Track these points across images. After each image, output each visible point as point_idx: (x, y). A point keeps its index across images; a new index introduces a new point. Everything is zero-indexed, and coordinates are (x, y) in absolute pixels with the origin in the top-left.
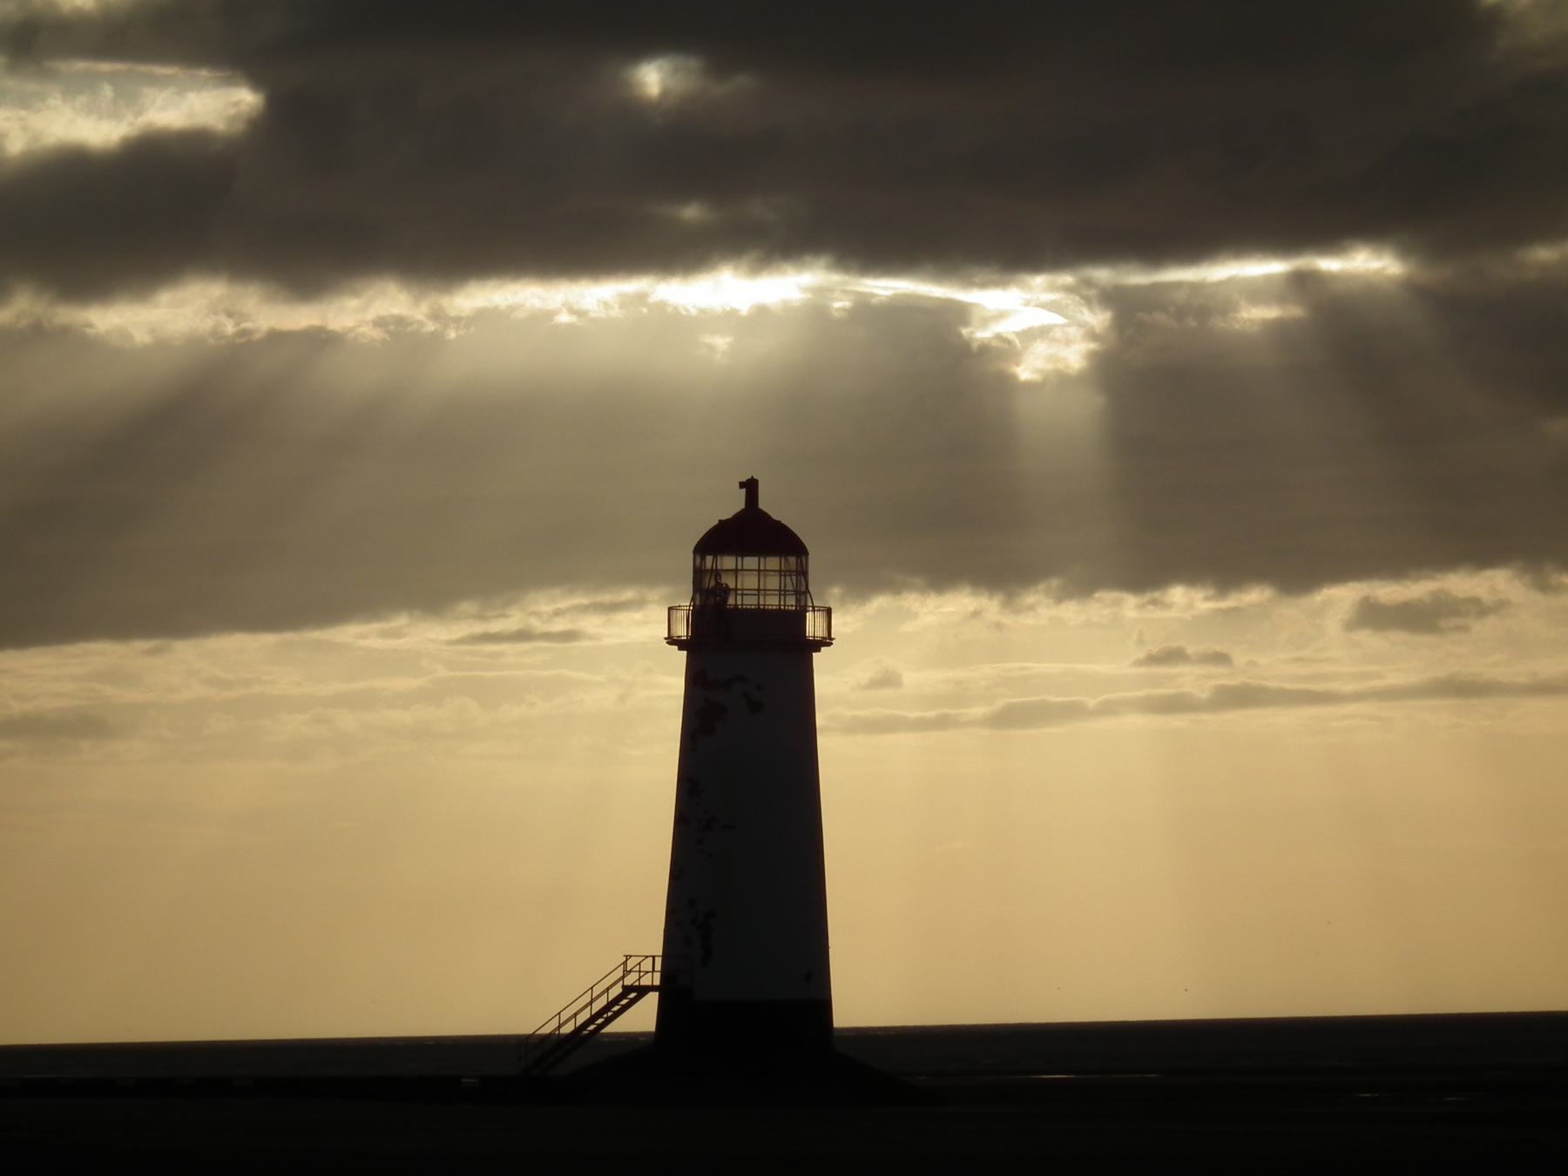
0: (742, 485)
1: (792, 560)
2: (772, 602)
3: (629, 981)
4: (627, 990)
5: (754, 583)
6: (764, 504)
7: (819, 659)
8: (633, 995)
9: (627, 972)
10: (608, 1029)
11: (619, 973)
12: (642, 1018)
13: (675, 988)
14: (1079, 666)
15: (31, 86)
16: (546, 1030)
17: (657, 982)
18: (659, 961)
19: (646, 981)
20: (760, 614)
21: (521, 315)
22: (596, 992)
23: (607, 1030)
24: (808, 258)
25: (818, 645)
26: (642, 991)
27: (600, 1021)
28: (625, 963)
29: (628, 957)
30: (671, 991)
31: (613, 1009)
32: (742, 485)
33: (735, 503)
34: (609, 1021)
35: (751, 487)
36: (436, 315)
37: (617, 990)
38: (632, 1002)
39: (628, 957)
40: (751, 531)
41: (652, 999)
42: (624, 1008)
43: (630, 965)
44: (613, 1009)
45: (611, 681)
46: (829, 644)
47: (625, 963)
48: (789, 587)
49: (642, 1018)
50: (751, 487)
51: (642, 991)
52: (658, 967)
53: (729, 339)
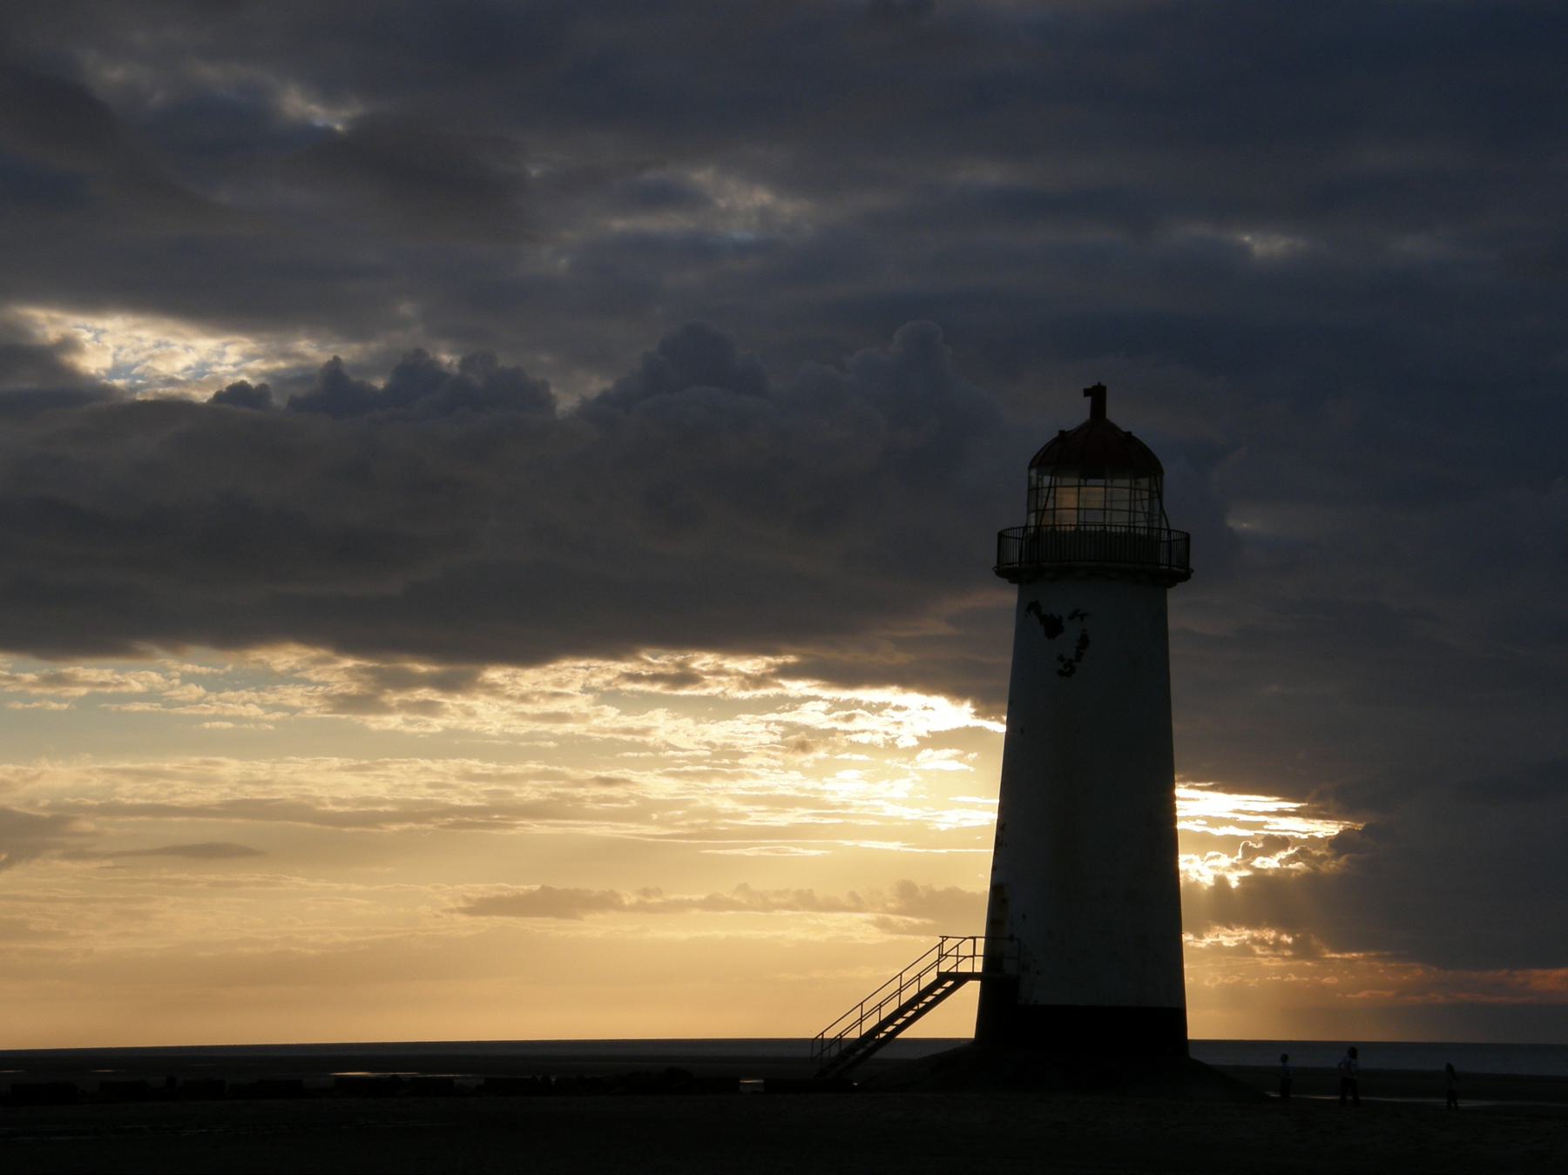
0: (1087, 392)
1: (1144, 482)
3: (945, 967)
4: (943, 977)
5: (1078, 503)
6: (1117, 414)
10: (901, 1035)
11: (934, 956)
12: (957, 1018)
17: (979, 968)
18: (981, 943)
19: (965, 967)
22: (867, 1007)
23: (901, 1035)
26: (960, 979)
28: (941, 945)
29: (945, 938)
30: (998, 983)
32: (1087, 392)
33: (1077, 414)
35: (1097, 395)
36: (1248, 866)
37: (931, 977)
40: (1095, 449)
41: (972, 989)
46: (1185, 576)
47: (941, 945)
48: (1139, 509)
49: (957, 1018)
50: (1097, 395)
51: (960, 979)
52: (980, 950)
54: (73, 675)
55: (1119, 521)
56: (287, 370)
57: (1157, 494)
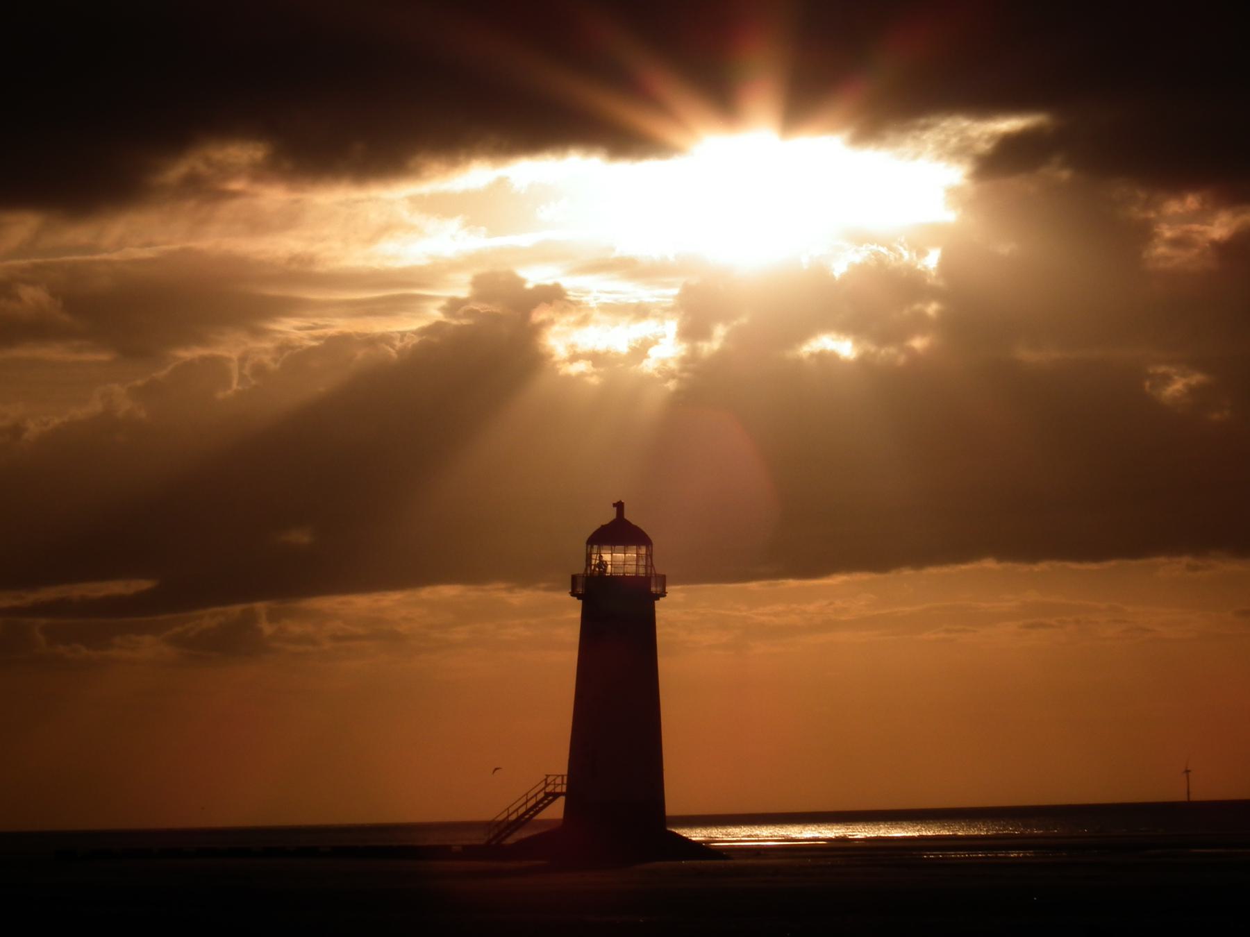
0: (614, 505)
1: (643, 550)
3: (549, 789)
4: (547, 795)
5: (618, 560)
6: (629, 516)
9: (547, 785)
11: (543, 785)
19: (558, 790)
22: (511, 810)
26: (556, 795)
30: (571, 796)
32: (614, 505)
33: (611, 515)
35: (619, 506)
37: (541, 795)
40: (620, 531)
41: (562, 800)
49: (556, 811)
50: (619, 506)
51: (556, 795)
54: (241, 269)
55: (631, 570)
56: (468, 326)
57: (649, 555)
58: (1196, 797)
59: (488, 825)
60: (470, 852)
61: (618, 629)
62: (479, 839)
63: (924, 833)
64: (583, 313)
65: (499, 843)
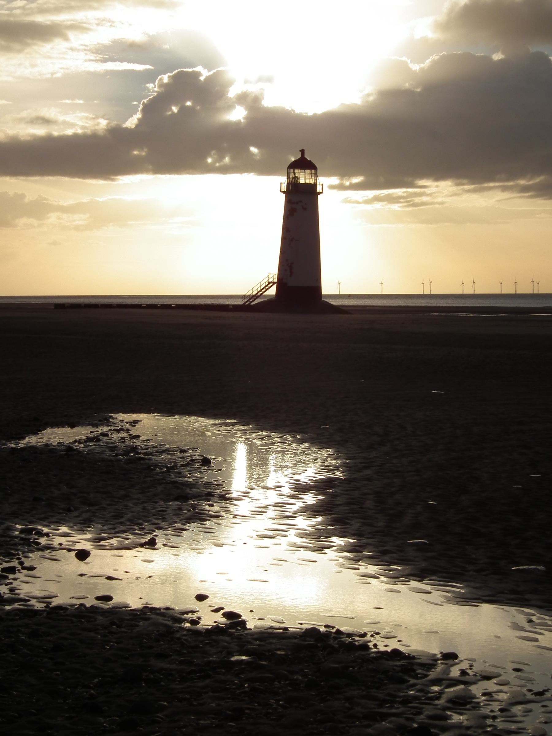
0: (300, 151)
1: (313, 171)
2: (308, 182)
3: (270, 281)
4: (269, 283)
5: (304, 178)
7: (320, 197)
8: (271, 284)
11: (267, 279)
13: (281, 283)
14: (184, 70)
15: (17, 46)
16: (249, 294)
20: (306, 184)
21: (459, 588)
24: (29, 138)
25: (319, 193)
27: (263, 291)
31: (266, 288)
32: (300, 151)
33: (299, 156)
34: (266, 291)
35: (303, 151)
38: (272, 286)
39: (270, 274)
41: (275, 285)
42: (268, 289)
43: (270, 277)
44: (266, 288)
45: (264, 197)
49: (272, 291)
50: (303, 151)
51: (274, 283)
53: (148, 85)
58: (540, 293)
59: (244, 297)
60: (236, 308)
61: (301, 209)
62: (240, 302)
63: (82, 432)
64: (297, 477)
65: (249, 307)
